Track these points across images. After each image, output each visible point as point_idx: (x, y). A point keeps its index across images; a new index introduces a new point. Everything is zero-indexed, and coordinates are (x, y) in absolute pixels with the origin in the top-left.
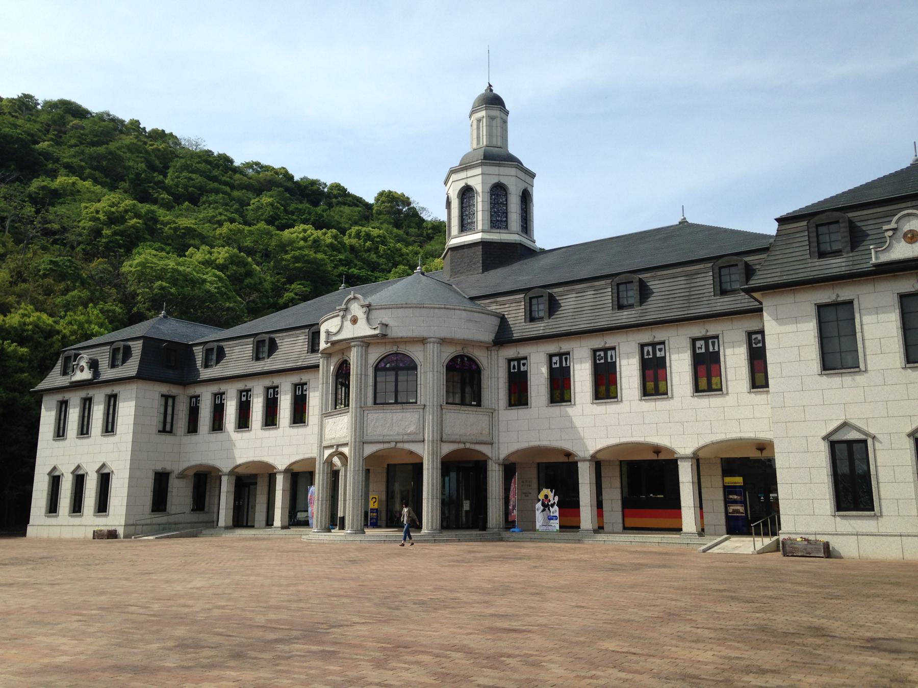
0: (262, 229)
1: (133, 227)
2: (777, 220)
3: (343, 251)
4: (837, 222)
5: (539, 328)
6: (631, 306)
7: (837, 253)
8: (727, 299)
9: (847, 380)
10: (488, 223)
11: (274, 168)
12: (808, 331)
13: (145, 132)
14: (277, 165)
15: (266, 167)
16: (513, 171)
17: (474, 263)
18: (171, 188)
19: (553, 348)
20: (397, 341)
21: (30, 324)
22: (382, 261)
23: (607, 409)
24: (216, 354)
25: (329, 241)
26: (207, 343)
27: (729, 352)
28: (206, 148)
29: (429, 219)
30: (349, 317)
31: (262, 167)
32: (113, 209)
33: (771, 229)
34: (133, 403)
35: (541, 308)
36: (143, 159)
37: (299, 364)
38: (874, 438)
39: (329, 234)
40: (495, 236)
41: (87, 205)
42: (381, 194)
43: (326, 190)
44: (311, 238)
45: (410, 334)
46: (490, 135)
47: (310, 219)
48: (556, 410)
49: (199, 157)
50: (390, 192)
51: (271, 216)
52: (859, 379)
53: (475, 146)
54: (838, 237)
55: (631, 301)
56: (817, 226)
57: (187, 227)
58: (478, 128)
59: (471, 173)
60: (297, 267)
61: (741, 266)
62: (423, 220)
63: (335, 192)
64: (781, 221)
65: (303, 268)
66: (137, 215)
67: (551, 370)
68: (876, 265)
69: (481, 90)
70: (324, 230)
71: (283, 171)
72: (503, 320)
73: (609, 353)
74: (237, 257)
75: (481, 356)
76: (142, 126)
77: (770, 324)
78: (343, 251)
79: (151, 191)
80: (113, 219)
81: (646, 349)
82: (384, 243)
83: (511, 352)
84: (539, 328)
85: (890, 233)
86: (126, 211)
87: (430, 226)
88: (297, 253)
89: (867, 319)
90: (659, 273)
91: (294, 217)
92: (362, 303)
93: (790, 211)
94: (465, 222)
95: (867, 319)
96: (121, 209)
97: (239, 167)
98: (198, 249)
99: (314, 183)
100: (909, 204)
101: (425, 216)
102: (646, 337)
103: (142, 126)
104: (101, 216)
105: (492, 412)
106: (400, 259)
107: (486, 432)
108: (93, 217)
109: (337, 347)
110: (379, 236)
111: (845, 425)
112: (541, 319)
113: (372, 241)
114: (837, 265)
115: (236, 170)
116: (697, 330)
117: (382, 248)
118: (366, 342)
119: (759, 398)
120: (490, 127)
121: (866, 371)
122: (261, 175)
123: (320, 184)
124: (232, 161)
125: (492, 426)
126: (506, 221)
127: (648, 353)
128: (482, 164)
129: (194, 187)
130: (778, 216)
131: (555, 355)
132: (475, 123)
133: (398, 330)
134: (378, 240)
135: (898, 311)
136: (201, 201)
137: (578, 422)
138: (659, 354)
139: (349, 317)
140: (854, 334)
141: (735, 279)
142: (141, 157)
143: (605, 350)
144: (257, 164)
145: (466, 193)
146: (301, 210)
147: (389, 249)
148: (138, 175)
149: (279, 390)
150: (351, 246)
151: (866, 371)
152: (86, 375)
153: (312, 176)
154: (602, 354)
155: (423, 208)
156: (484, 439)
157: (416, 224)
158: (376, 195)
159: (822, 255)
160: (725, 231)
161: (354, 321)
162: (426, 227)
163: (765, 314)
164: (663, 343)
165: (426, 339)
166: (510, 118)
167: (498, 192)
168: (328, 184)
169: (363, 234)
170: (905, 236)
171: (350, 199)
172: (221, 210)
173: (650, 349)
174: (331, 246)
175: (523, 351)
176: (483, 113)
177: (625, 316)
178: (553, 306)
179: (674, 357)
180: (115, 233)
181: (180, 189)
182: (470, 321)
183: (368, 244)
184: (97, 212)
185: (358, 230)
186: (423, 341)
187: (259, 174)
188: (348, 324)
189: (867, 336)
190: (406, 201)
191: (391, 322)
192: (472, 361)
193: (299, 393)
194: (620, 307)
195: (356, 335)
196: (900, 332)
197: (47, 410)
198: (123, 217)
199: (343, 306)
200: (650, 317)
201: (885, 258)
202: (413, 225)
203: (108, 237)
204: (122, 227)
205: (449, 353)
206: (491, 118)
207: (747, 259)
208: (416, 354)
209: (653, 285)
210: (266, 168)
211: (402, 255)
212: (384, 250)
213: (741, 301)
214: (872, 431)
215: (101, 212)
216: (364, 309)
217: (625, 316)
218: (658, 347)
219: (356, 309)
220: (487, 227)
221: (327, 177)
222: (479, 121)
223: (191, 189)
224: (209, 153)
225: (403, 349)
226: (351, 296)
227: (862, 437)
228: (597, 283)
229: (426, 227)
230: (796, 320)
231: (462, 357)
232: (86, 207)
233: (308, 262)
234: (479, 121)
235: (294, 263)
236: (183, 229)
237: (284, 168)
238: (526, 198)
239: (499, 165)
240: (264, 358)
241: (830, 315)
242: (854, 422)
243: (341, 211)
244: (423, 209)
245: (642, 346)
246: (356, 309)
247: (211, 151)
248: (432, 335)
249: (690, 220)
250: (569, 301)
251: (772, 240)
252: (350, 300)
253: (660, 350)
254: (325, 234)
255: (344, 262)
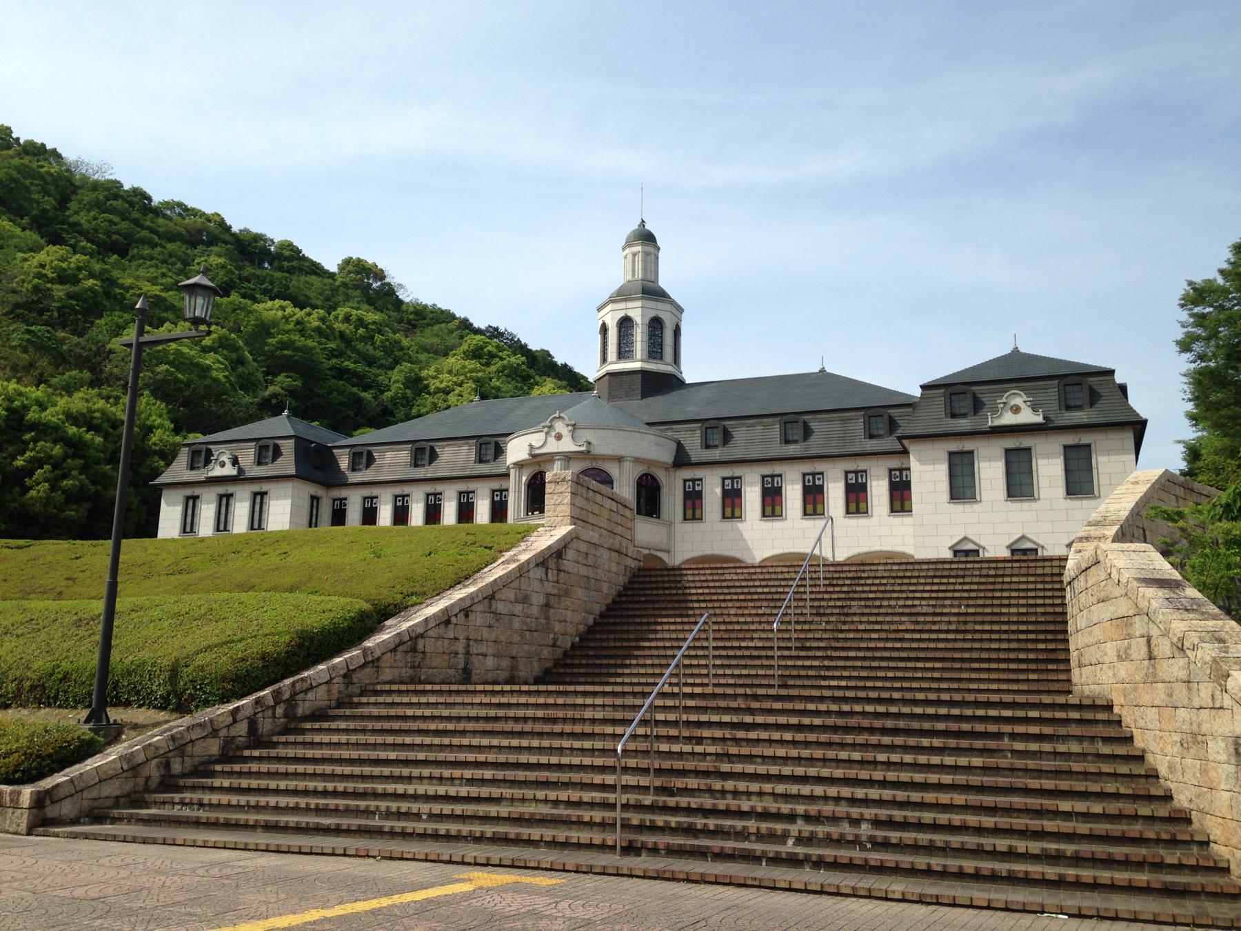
0: (237, 302)
1: (91, 289)
2: (921, 387)
3: (332, 338)
4: (965, 393)
5: (716, 454)
6: (796, 442)
7: (964, 416)
8: (874, 442)
9: (968, 507)
10: (646, 352)
11: (204, 213)
12: (940, 472)
13: (19, 144)
14: (208, 210)
15: (193, 210)
16: (668, 307)
17: (634, 390)
18: (88, 232)
19: (727, 472)
20: (597, 458)
21: (98, 410)
22: (379, 354)
23: (773, 527)
24: (364, 458)
25: (315, 324)
26: (355, 445)
27: (748, 489)
28: (113, 177)
29: (407, 300)
30: (553, 434)
31: (186, 209)
32: (64, 265)
33: (917, 392)
34: (289, 502)
35: (717, 437)
36: (39, 188)
37: (467, 473)
38: (984, 548)
39: (315, 315)
40: (653, 366)
41: (26, 256)
42: (348, 261)
43: (272, 249)
44: (294, 319)
45: (610, 453)
46: (645, 270)
47: (271, 290)
48: (728, 525)
49: (107, 189)
50: (359, 260)
51: (225, 282)
52: (976, 507)
53: (629, 277)
54: (965, 404)
55: (796, 438)
56: (951, 394)
57: (156, 295)
58: (634, 261)
59: (630, 304)
60: (284, 355)
61: (886, 417)
62: (401, 302)
63: (287, 253)
64: (923, 387)
65: (294, 356)
66: (92, 275)
67: (493, 503)
68: (991, 427)
69: (635, 226)
70: (308, 310)
71: (218, 219)
72: (680, 447)
73: (776, 479)
74: (227, 339)
75: (661, 475)
76: (14, 135)
77: (914, 463)
78: (332, 338)
79: (65, 235)
80: (64, 278)
81: (807, 477)
82: (380, 332)
83: (688, 473)
84: (716, 454)
85: (1002, 405)
86: (79, 269)
87: (411, 309)
88: (285, 337)
89: (982, 465)
90: (819, 416)
91: (251, 286)
92: (568, 422)
93: (930, 380)
94: (623, 350)
95: (982, 465)
96: (72, 265)
97: (157, 207)
98: (176, 325)
99: (258, 238)
100: (1013, 385)
101: (402, 295)
102: (808, 467)
103: (14, 135)
104: (48, 272)
105: (670, 524)
106: (401, 353)
107: (665, 541)
108: (39, 273)
109: (538, 459)
110: (374, 323)
111: (965, 539)
112: (716, 447)
113: (366, 327)
114: (964, 424)
115: (157, 212)
116: (850, 465)
117: (378, 338)
118: (568, 457)
119: (899, 521)
120: (645, 262)
121: (981, 501)
122: (187, 221)
123: (265, 240)
124: (150, 199)
125: (670, 536)
126: (661, 353)
127: (809, 481)
128: (642, 298)
129: (117, 233)
130: (922, 384)
131: (689, 480)
132: (630, 257)
133: (600, 449)
134: (374, 327)
135: (1003, 461)
136: (130, 254)
137: (746, 536)
138: (817, 482)
139: (553, 434)
140: (1091, 470)
141: (881, 426)
142: (37, 185)
143: (772, 476)
144: (180, 205)
145: (625, 323)
146: (258, 277)
147: (387, 340)
148: (44, 211)
149: (347, 502)
150: (340, 332)
151: (981, 501)
152: (229, 470)
153: (255, 229)
154: (898, 473)
155: (400, 285)
156: (662, 546)
157: (393, 305)
158: (340, 262)
159: (953, 416)
160: (865, 384)
161: (559, 437)
162: (407, 311)
163: (912, 457)
164: (822, 473)
165: (622, 457)
166: (661, 254)
167: (656, 324)
168: (276, 241)
169: (354, 318)
170: (1012, 407)
171: (306, 264)
172: (164, 270)
173: (811, 477)
174: (318, 330)
175: (698, 473)
176: (639, 248)
177: (792, 450)
178: (727, 437)
179: (831, 485)
180: (69, 296)
181: (101, 236)
182: (657, 444)
183: (361, 331)
184: (43, 266)
185: (347, 313)
186: (620, 459)
187: (184, 219)
188: (552, 440)
189: (982, 477)
190: (380, 275)
191: (593, 441)
192: (653, 478)
193: (368, 505)
194: (787, 442)
195: (560, 450)
196: (1063, 472)
197: (168, 504)
198: (75, 276)
199: (547, 423)
200: (814, 452)
201: (998, 422)
202: (390, 306)
203: (60, 300)
204: (77, 289)
205: (639, 470)
206: (646, 254)
207: (890, 411)
208: (613, 469)
209: (814, 425)
210: (195, 212)
211: (402, 349)
212: (382, 342)
213: (890, 443)
214: (983, 544)
215: (47, 267)
216: (570, 428)
217: (792, 450)
218: (817, 476)
219: (560, 427)
220: (645, 357)
221: (276, 232)
222: (634, 255)
223: (114, 237)
224: (117, 184)
225: (600, 465)
226: (557, 415)
227: (976, 548)
228: (765, 420)
229: (407, 311)
230: (934, 462)
231: (646, 475)
232: (25, 260)
233: (297, 349)
234: (634, 255)
235: (281, 349)
236: (151, 297)
237: (219, 215)
238: (677, 332)
239: (657, 300)
240: (267, 463)
241: (958, 460)
242: (970, 537)
243: (307, 283)
244: (401, 286)
245: (804, 475)
246: (560, 427)
247: (119, 182)
248: (628, 454)
249: (828, 370)
250: (740, 434)
251: (917, 400)
252: (556, 418)
253: (819, 479)
254: (309, 314)
255: (336, 353)
